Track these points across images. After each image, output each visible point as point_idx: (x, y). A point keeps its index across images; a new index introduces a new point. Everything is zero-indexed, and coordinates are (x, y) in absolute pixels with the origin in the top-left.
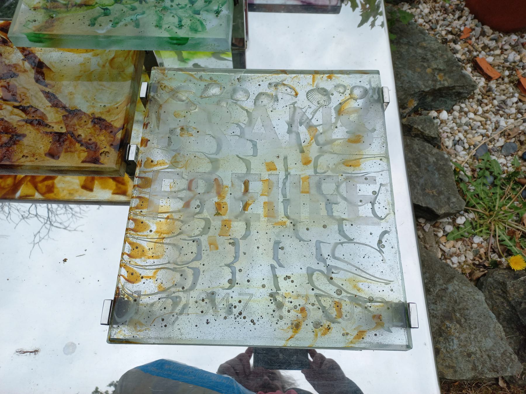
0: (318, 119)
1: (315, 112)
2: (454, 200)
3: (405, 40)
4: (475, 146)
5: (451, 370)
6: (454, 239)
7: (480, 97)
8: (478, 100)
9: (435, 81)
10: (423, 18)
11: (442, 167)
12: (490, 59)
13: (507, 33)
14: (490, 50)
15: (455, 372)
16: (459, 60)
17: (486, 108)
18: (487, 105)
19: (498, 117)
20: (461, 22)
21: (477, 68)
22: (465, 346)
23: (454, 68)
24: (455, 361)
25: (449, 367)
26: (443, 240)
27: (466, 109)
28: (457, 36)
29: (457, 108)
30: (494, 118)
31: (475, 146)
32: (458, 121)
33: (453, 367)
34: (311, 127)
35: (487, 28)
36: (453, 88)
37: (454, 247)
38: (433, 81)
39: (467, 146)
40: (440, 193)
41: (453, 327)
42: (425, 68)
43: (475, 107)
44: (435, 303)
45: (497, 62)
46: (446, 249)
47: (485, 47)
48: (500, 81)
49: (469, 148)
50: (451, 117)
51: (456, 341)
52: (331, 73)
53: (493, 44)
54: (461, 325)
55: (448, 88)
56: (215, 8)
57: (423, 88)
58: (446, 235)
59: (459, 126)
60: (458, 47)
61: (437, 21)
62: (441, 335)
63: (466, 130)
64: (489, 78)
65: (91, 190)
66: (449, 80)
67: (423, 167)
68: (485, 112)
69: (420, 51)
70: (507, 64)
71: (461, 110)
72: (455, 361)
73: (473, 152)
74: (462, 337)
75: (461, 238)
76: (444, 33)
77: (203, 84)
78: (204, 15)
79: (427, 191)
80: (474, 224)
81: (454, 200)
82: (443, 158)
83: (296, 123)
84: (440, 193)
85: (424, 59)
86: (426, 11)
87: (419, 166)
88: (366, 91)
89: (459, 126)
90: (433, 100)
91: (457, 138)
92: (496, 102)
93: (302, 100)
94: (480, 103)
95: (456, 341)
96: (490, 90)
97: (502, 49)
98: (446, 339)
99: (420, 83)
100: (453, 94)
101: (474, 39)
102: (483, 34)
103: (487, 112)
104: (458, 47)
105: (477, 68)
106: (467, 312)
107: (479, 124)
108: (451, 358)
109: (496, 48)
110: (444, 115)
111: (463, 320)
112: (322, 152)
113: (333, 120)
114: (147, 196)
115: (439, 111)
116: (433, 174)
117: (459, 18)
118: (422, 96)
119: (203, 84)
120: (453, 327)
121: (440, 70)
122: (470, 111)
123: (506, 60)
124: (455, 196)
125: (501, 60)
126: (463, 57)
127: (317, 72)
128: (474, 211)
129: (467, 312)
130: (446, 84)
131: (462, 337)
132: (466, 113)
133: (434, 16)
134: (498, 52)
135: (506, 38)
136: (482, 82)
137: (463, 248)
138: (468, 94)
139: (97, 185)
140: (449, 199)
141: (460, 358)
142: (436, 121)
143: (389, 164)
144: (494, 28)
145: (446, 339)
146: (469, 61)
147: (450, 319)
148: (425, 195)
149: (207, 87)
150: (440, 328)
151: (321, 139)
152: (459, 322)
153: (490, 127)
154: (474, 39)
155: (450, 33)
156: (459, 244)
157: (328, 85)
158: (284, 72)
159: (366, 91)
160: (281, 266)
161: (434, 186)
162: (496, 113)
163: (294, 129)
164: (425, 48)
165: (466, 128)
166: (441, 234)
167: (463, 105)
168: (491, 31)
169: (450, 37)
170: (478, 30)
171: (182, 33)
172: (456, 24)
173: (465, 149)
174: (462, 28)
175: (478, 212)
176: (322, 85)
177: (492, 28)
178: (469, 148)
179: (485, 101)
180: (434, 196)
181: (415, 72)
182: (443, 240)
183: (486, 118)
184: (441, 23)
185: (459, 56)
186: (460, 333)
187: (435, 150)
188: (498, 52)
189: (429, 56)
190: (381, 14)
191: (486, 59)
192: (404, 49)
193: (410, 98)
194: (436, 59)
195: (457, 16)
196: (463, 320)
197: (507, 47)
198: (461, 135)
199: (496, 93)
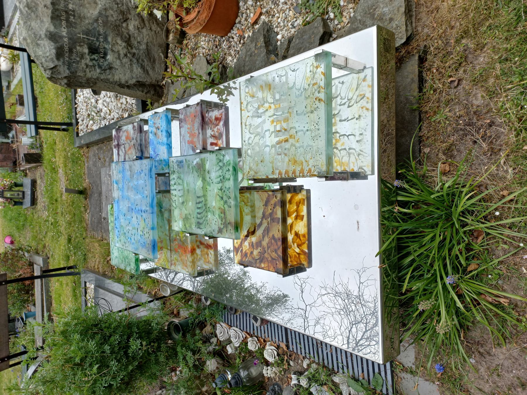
0: (256, 105)
1: (254, 107)
2: (316, 24)
3: (242, 68)
4: (295, 15)
5: (400, 9)
6: (341, 18)
7: (270, 17)
8: (272, 17)
9: (261, 46)
10: (233, 60)
11: (301, 33)
12: (252, 15)
13: (238, 8)
14: (248, 16)
15: (401, 6)
16: (253, 33)
17: (276, 12)
18: (274, 12)
19: (280, 4)
20: (235, 37)
21: (256, 22)
22: (386, 4)
23: (255, 37)
24: (394, 8)
25: (398, 10)
26: (342, 24)
27: (277, 24)
28: (242, 37)
29: (276, 30)
30: (281, 6)
31: (295, 15)
32: (282, 27)
33: (398, 9)
34: (259, 108)
35: (237, 21)
36: (264, 35)
37: (346, 17)
38: (261, 48)
39: (295, 19)
40: (313, 33)
41: (377, 13)
42: (255, 54)
43: (275, 19)
44: (366, 25)
45: (253, 11)
46: (347, 21)
47: (246, 20)
48: (262, 7)
49: (296, 18)
50: (280, 32)
51: (384, 10)
52: (241, 103)
53: (244, 15)
54: (376, 8)
55: (265, 38)
56: (222, 157)
57: (264, 53)
58: (339, 23)
59: (284, 26)
60: (246, 36)
61: (235, 50)
62: (382, 19)
63: (286, 23)
64: (261, 14)
65: (303, 216)
66: (261, 38)
67: (301, 46)
68: (278, 12)
69: (247, 59)
70: (254, 4)
71: (277, 27)
72: (394, 8)
73: (298, 15)
74: (382, 6)
75: (341, 13)
76: (240, 46)
77: (247, 156)
78: (225, 162)
79: (312, 41)
80: (334, 7)
81: (316, 24)
82: (297, 35)
83: (258, 115)
84: (313, 33)
85: (251, 56)
86: (230, 58)
87: (301, 48)
88: (247, 87)
89: (284, 26)
90: (272, 46)
91: (291, 27)
92: (273, 7)
93: (250, 114)
94: (273, 16)
95: (384, 10)
96: (267, 12)
97: (247, 10)
98: (384, 15)
99: (262, 55)
100: (268, 33)
101: (243, 27)
102: (240, 22)
103: (277, 11)
104: (246, 36)
105: (256, 22)
106: (370, 6)
107: (284, 14)
108: (393, 11)
109: (246, 13)
110: (279, 37)
111: (374, 7)
112: (267, 102)
113: (256, 99)
114: (284, 171)
115: (278, 40)
116: (304, 39)
117: (233, 38)
118: (269, 52)
119: (247, 156)
120: (377, 13)
121: (256, 45)
122: (278, 20)
123: (252, 6)
124: (314, 24)
125: (252, 8)
126: (251, 31)
127: (241, 109)
128: (327, 8)
129: (370, 6)
130: (263, 40)
131: (382, 6)
132: (279, 23)
133: (233, 53)
134: (248, 11)
135: (241, 8)
136: (263, 17)
137: (347, 11)
138: (268, 25)
139: (302, 214)
140: (316, 27)
141: (393, 5)
142: (282, 41)
143: (268, 72)
144: (237, 16)
145: (384, 15)
146: (253, 28)
147: (374, 14)
148: (314, 42)
149: (248, 155)
150: (379, 20)
151: (262, 102)
152: (375, 10)
153: (285, 7)
154: (243, 27)
155: (240, 41)
156: (344, 14)
157: (245, 103)
158: (241, 123)
159: (247, 87)
160: (348, 118)
161: (310, 37)
162: (278, 5)
163: (259, 115)
164: (246, 56)
165: (286, 22)
166: (339, 26)
167: (275, 26)
168: (238, 18)
169: (242, 41)
170: (238, 25)
171: (231, 169)
172: (235, 40)
173: (296, 21)
174: (238, 35)
175: (327, 6)
176: (245, 106)
177: (237, 18)
178: (296, 18)
179: (272, 13)
180: (314, 37)
181: (257, 60)
182: (342, 24)
183: (281, 10)
184: (235, 48)
185: (251, 34)
186: (380, 8)
187: (294, 40)
188: (248, 11)
189: (248, 53)
190: (229, 84)
191: (252, 17)
192: (247, 68)
193: (270, 60)
194: (250, 49)
195: (232, 40)
196: (374, 7)
197: (245, 7)
198: (289, 24)
199: (268, 8)
